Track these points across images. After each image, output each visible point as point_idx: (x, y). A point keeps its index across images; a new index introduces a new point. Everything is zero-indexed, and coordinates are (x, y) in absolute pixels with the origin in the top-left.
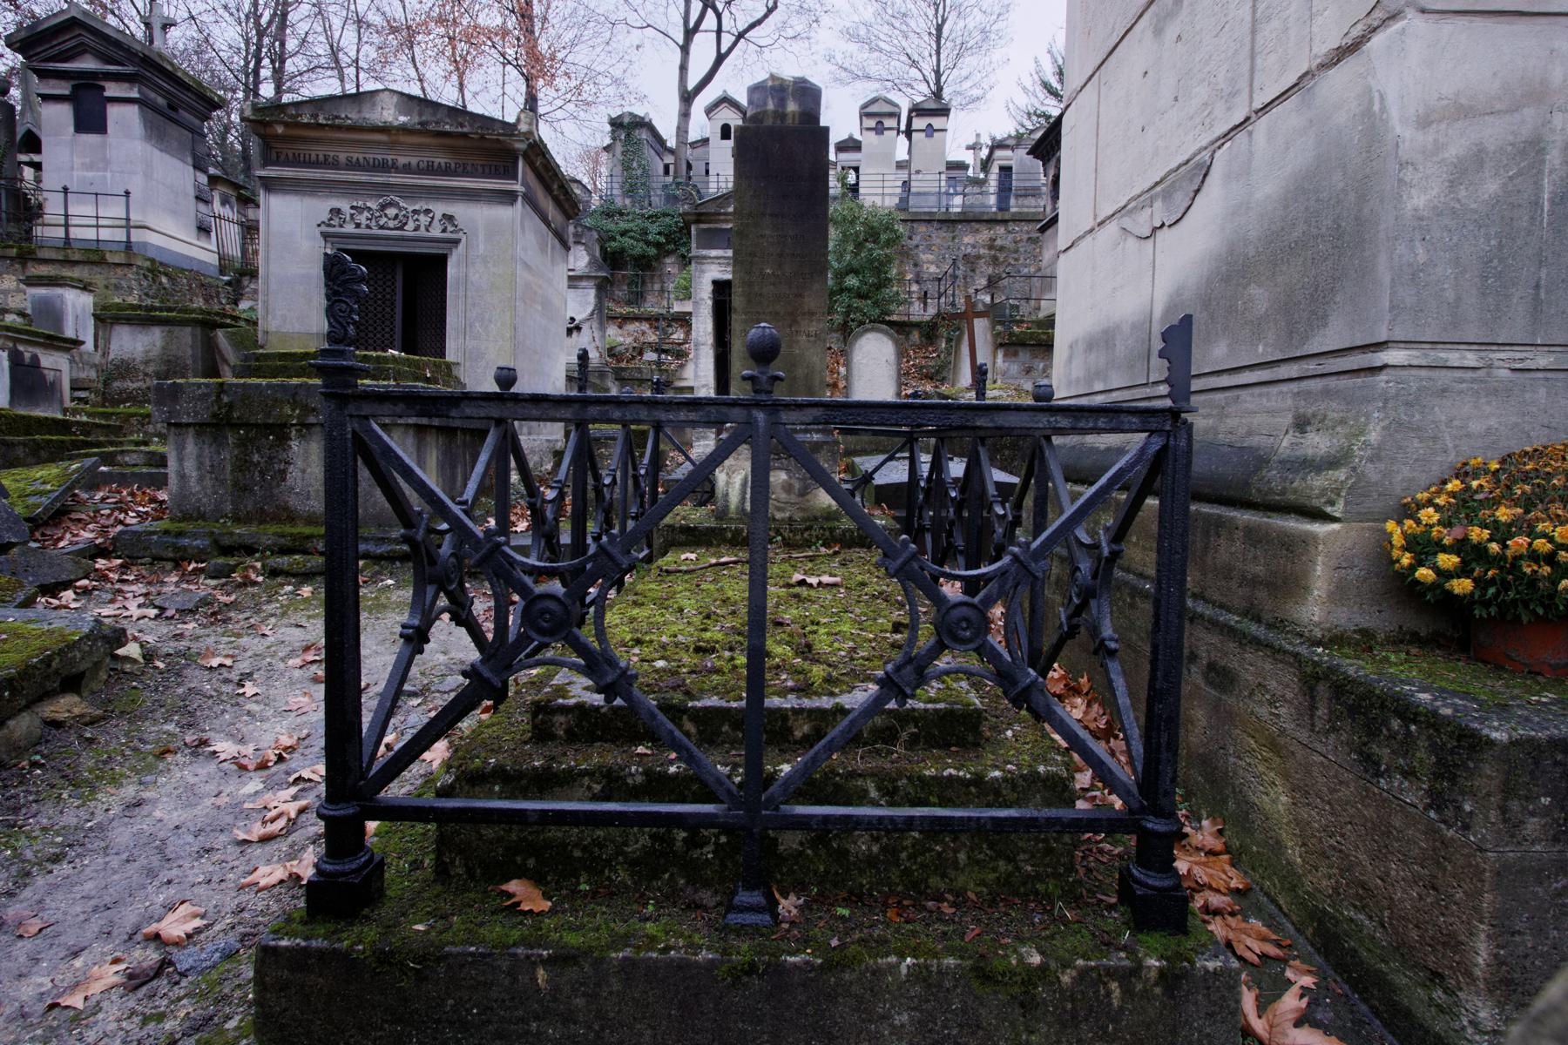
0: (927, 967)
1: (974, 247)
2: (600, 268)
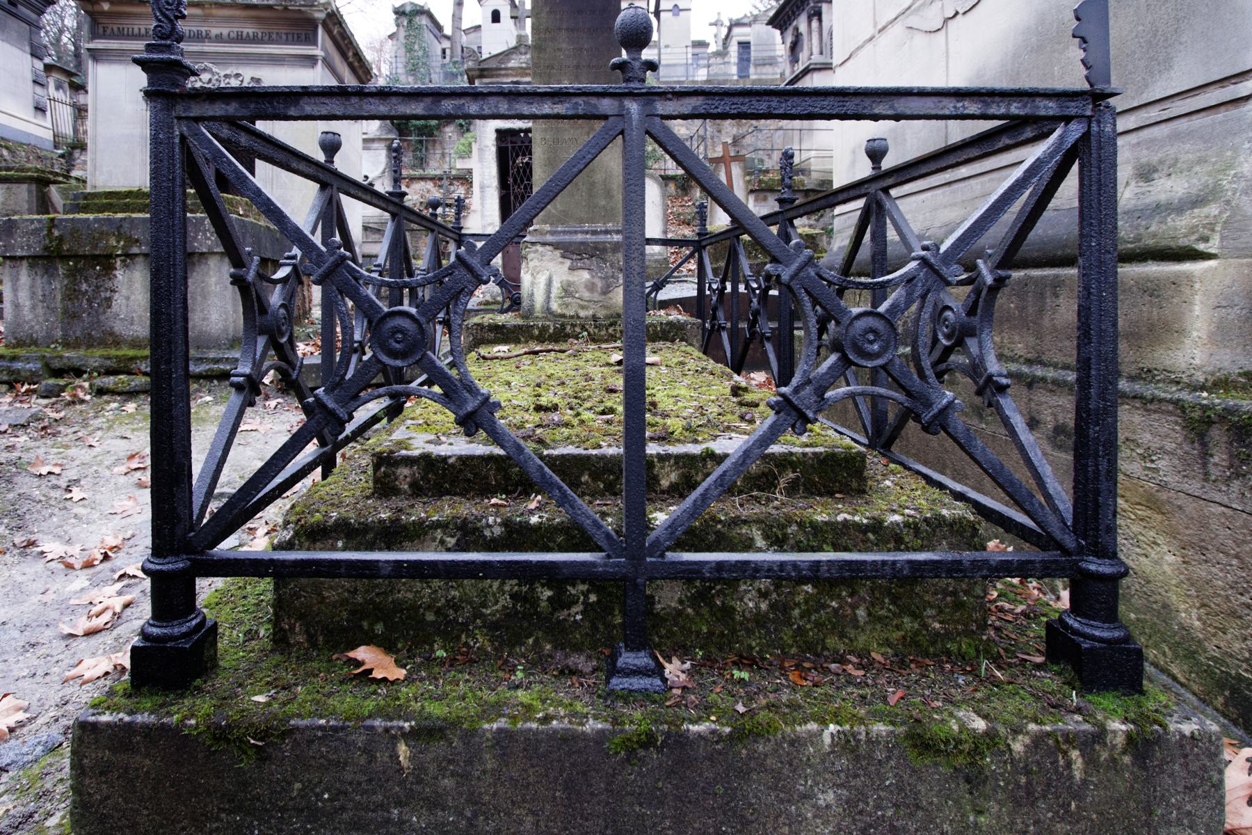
0: (854, 735)
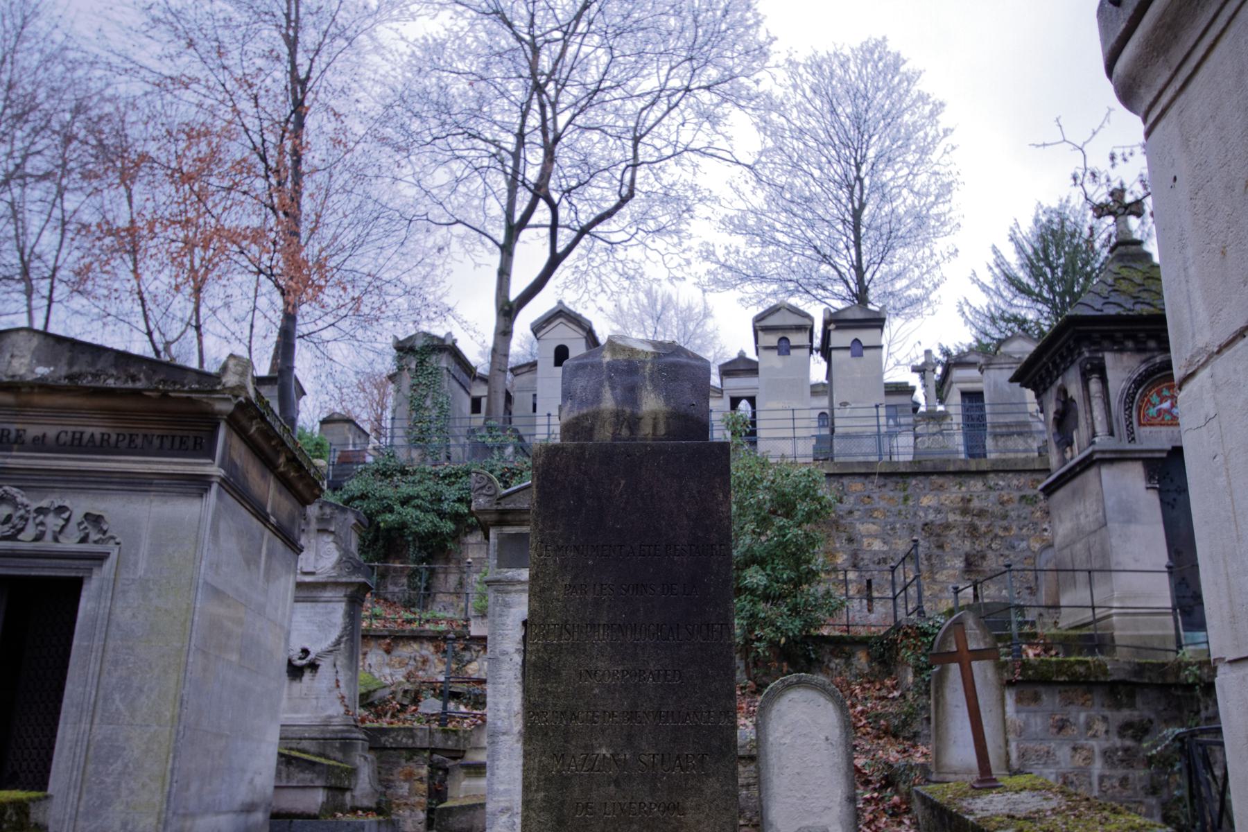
1: (938, 511)
2: (356, 569)
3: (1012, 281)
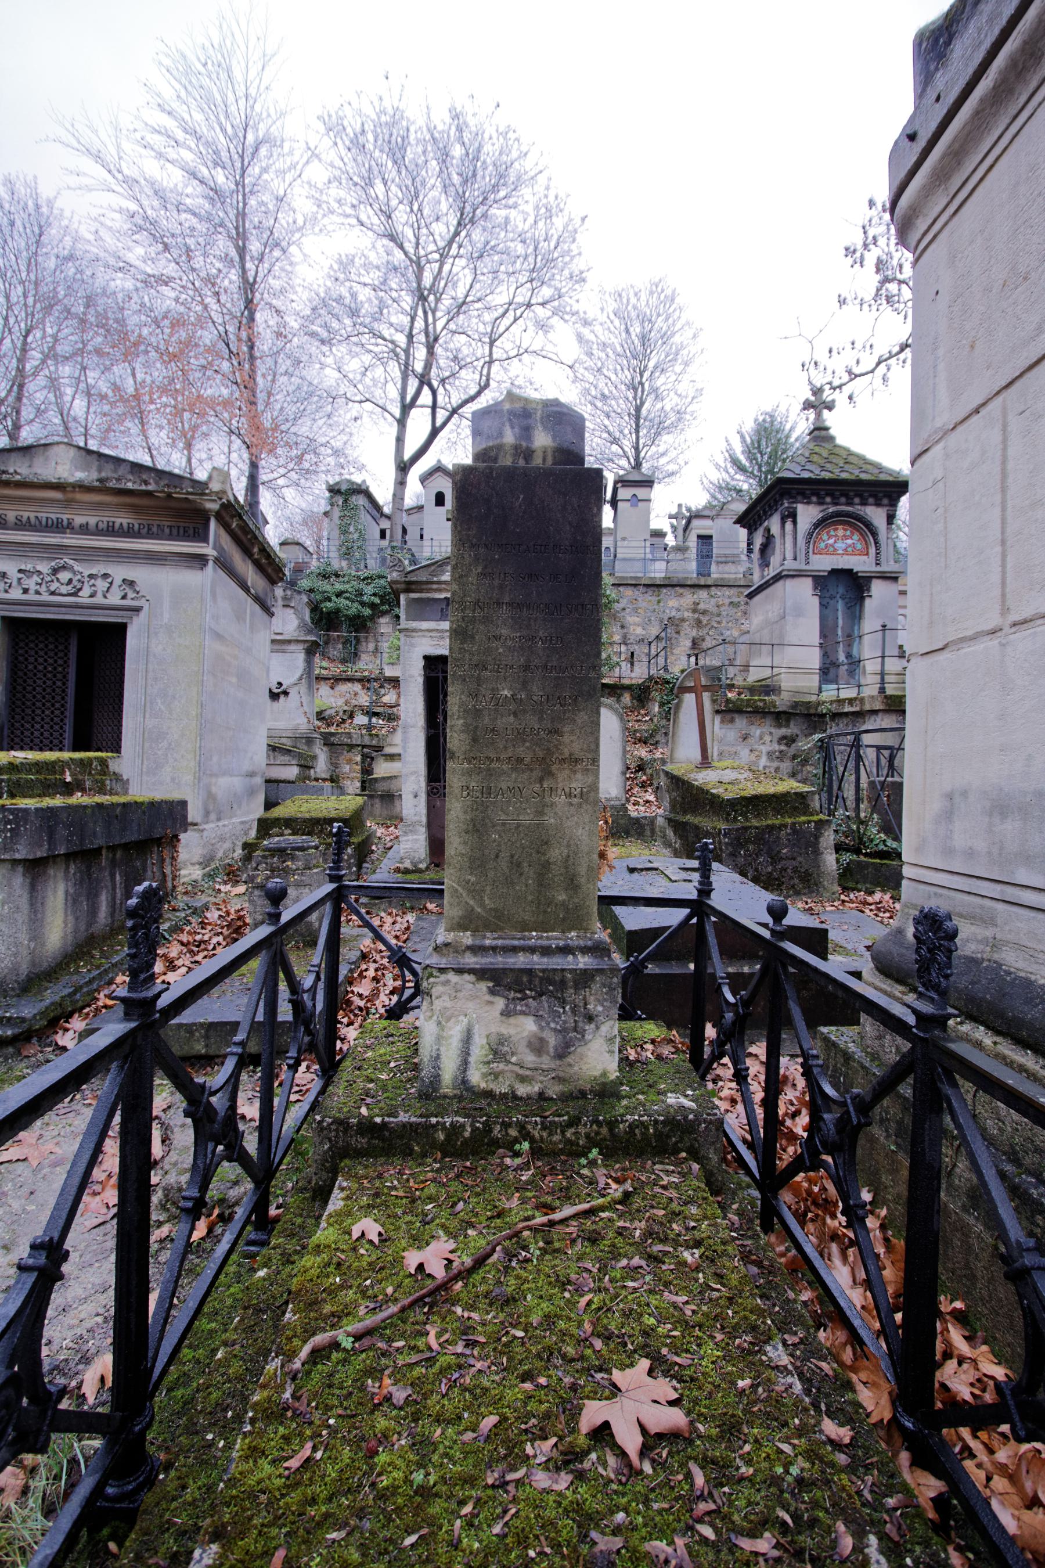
2: (310, 632)
3: (735, 462)
